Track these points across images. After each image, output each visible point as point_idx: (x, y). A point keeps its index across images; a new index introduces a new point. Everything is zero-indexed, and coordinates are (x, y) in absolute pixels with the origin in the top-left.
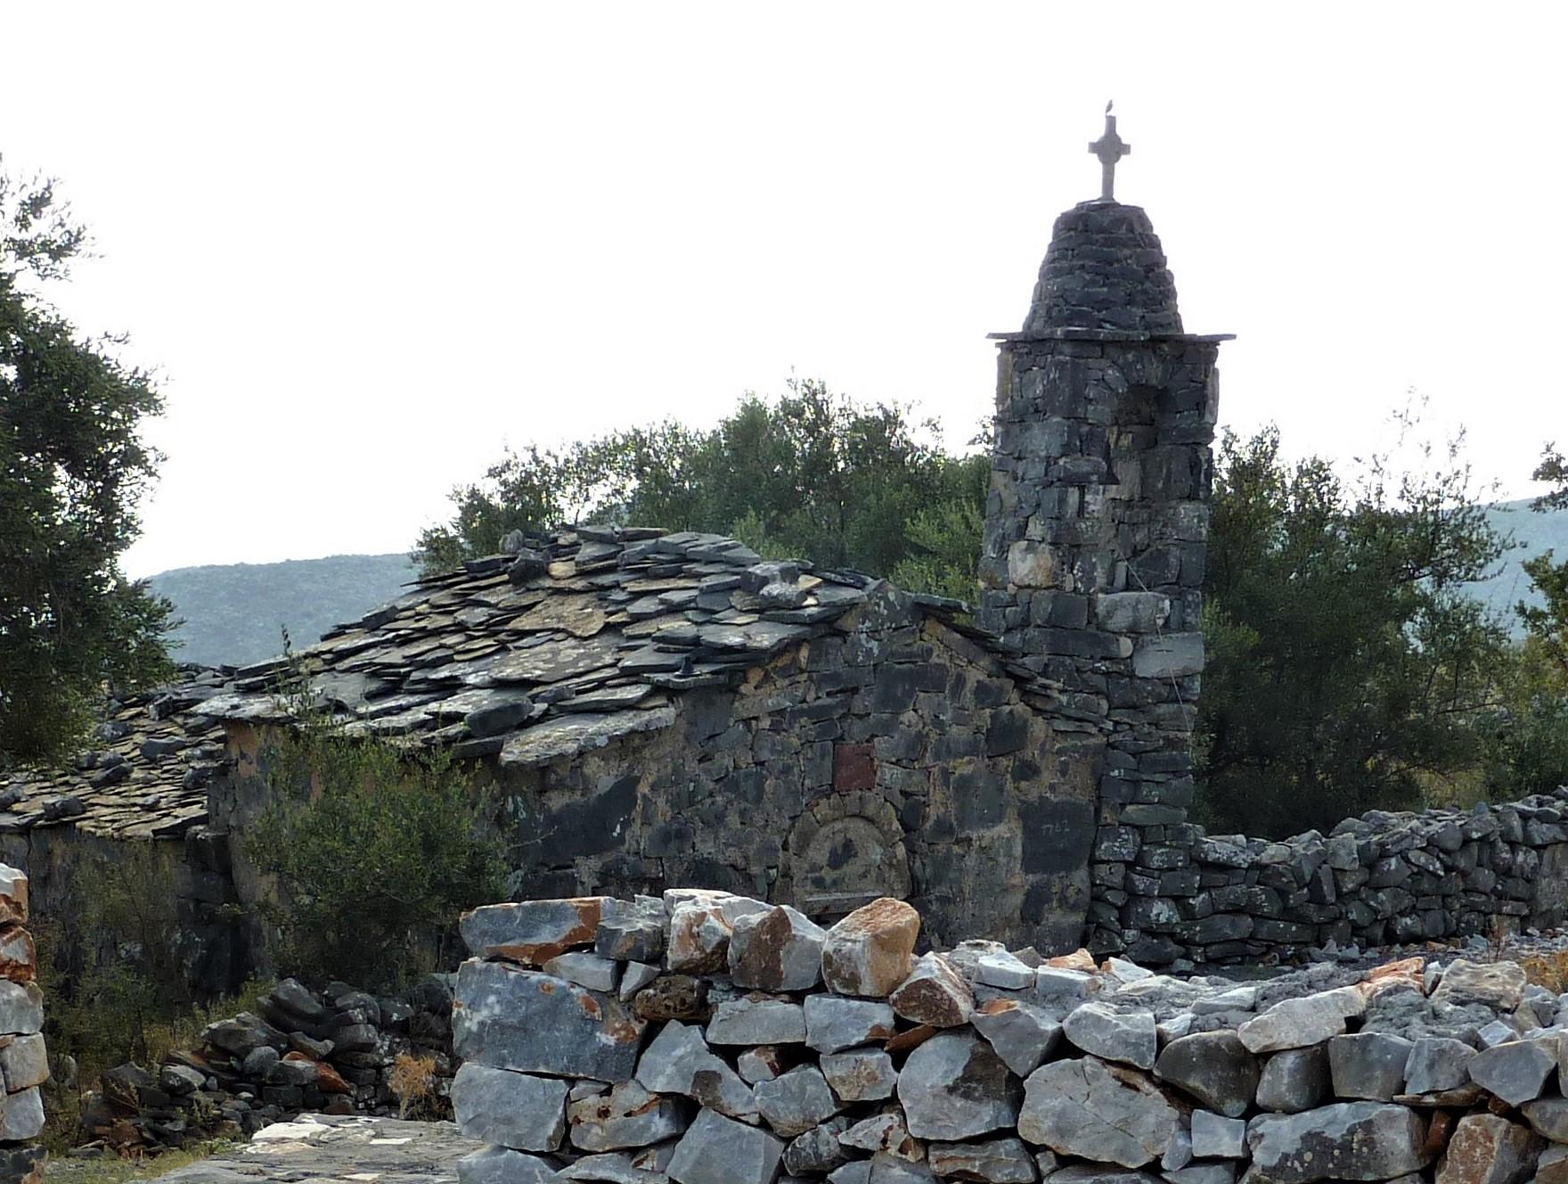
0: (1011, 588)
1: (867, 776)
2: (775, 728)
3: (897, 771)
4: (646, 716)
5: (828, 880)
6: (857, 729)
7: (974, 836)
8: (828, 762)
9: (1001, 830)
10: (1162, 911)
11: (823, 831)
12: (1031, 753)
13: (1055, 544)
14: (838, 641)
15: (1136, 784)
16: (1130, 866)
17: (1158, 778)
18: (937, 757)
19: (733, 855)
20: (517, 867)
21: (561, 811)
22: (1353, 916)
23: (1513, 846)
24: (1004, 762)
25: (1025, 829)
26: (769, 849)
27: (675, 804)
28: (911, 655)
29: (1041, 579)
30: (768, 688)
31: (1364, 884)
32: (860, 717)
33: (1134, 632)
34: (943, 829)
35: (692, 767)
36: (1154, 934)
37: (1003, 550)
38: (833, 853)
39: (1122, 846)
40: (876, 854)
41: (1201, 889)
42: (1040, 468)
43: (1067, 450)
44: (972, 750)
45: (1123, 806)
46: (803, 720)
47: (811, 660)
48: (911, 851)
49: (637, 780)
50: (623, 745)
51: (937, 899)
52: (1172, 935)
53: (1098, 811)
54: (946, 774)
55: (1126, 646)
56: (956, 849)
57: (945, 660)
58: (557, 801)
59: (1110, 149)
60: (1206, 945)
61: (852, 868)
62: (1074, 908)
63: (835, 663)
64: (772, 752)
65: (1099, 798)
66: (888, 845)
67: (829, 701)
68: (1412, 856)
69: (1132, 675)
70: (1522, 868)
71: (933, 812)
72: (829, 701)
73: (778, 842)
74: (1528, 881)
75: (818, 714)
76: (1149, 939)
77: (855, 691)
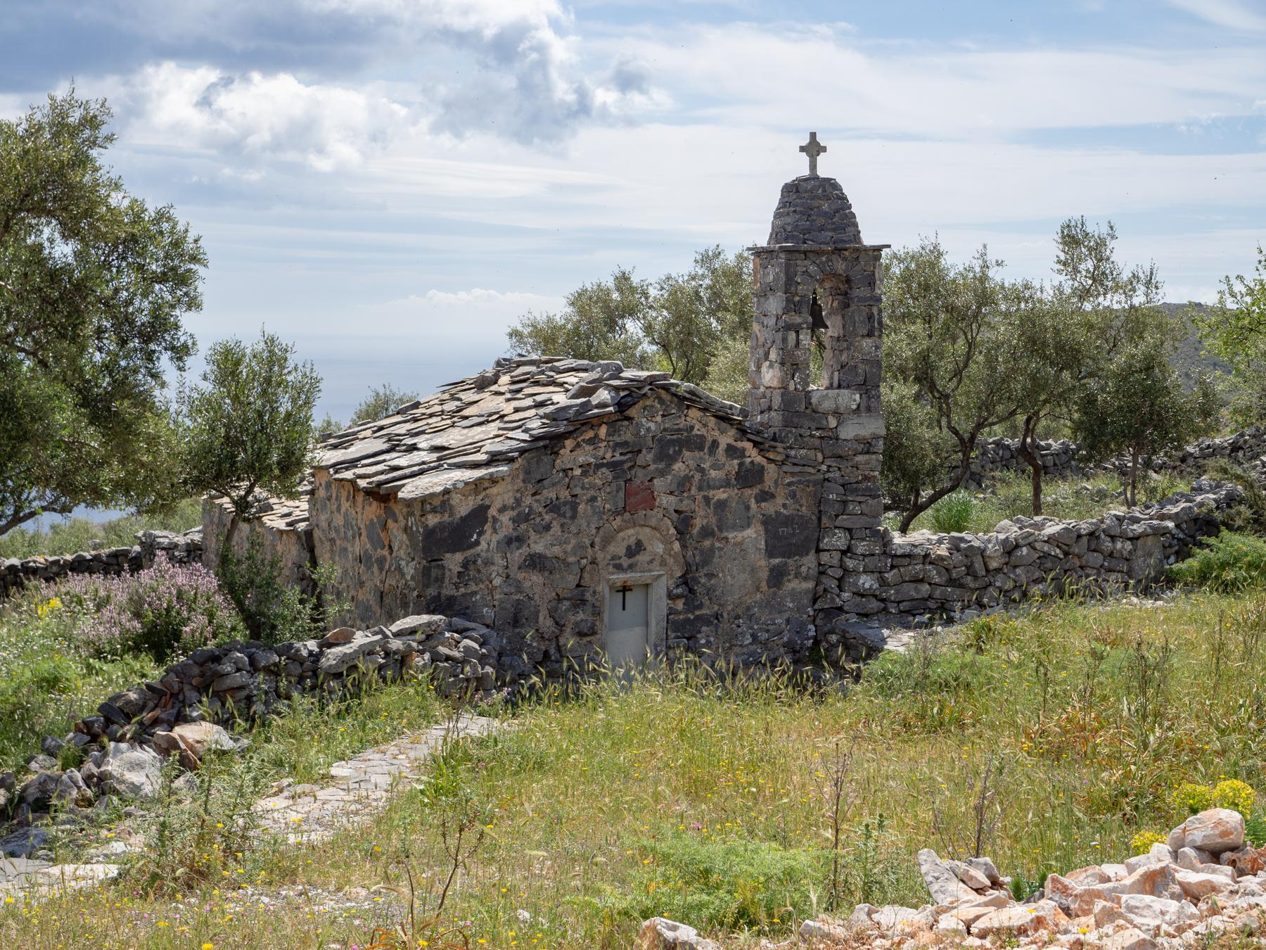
0: (762, 389)
1: (650, 502)
2: (584, 474)
3: (672, 498)
4: (492, 470)
5: (625, 565)
6: (640, 476)
7: (730, 536)
8: (622, 494)
9: (750, 532)
10: (867, 582)
11: (621, 534)
12: (768, 483)
13: (782, 364)
14: (626, 423)
15: (845, 503)
16: (844, 553)
17: (859, 499)
18: (700, 489)
19: (556, 550)
20: (413, 559)
21: (435, 527)
22: (998, 584)
23: (1113, 538)
24: (748, 492)
25: (767, 531)
26: (580, 546)
27: (516, 521)
28: (679, 430)
29: (775, 384)
30: (578, 451)
31: (1007, 564)
32: (644, 467)
33: (836, 413)
34: (706, 532)
35: (528, 500)
36: (862, 596)
37: (759, 367)
38: (629, 548)
39: (838, 540)
40: (660, 548)
41: (893, 567)
42: (774, 320)
43: (786, 311)
44: (726, 484)
45: (837, 516)
46: (604, 470)
47: (608, 434)
48: (684, 546)
49: (488, 507)
50: (477, 485)
51: (706, 575)
52: (875, 596)
53: (819, 519)
54: (707, 500)
55: (833, 422)
56: (717, 545)
57: (703, 431)
58: (432, 520)
59: (813, 149)
60: (899, 602)
61: (642, 558)
62: (806, 579)
63: (627, 436)
64: (583, 488)
65: (820, 512)
66: (667, 542)
67: (622, 458)
68: (1038, 545)
69: (837, 439)
70: (1121, 552)
71: (698, 523)
72: (622, 458)
73: (588, 542)
74: (1127, 560)
75: (613, 466)
76: (858, 599)
77: (640, 451)
